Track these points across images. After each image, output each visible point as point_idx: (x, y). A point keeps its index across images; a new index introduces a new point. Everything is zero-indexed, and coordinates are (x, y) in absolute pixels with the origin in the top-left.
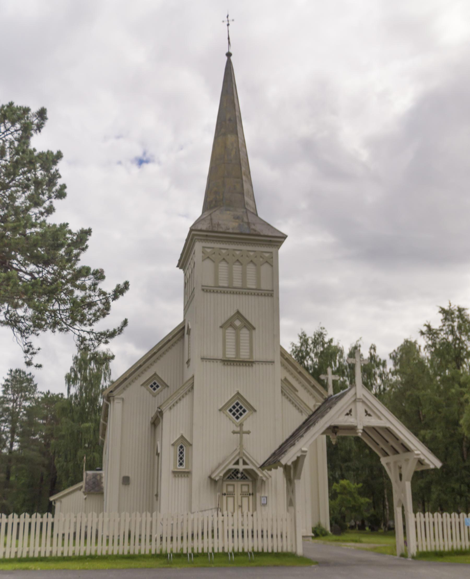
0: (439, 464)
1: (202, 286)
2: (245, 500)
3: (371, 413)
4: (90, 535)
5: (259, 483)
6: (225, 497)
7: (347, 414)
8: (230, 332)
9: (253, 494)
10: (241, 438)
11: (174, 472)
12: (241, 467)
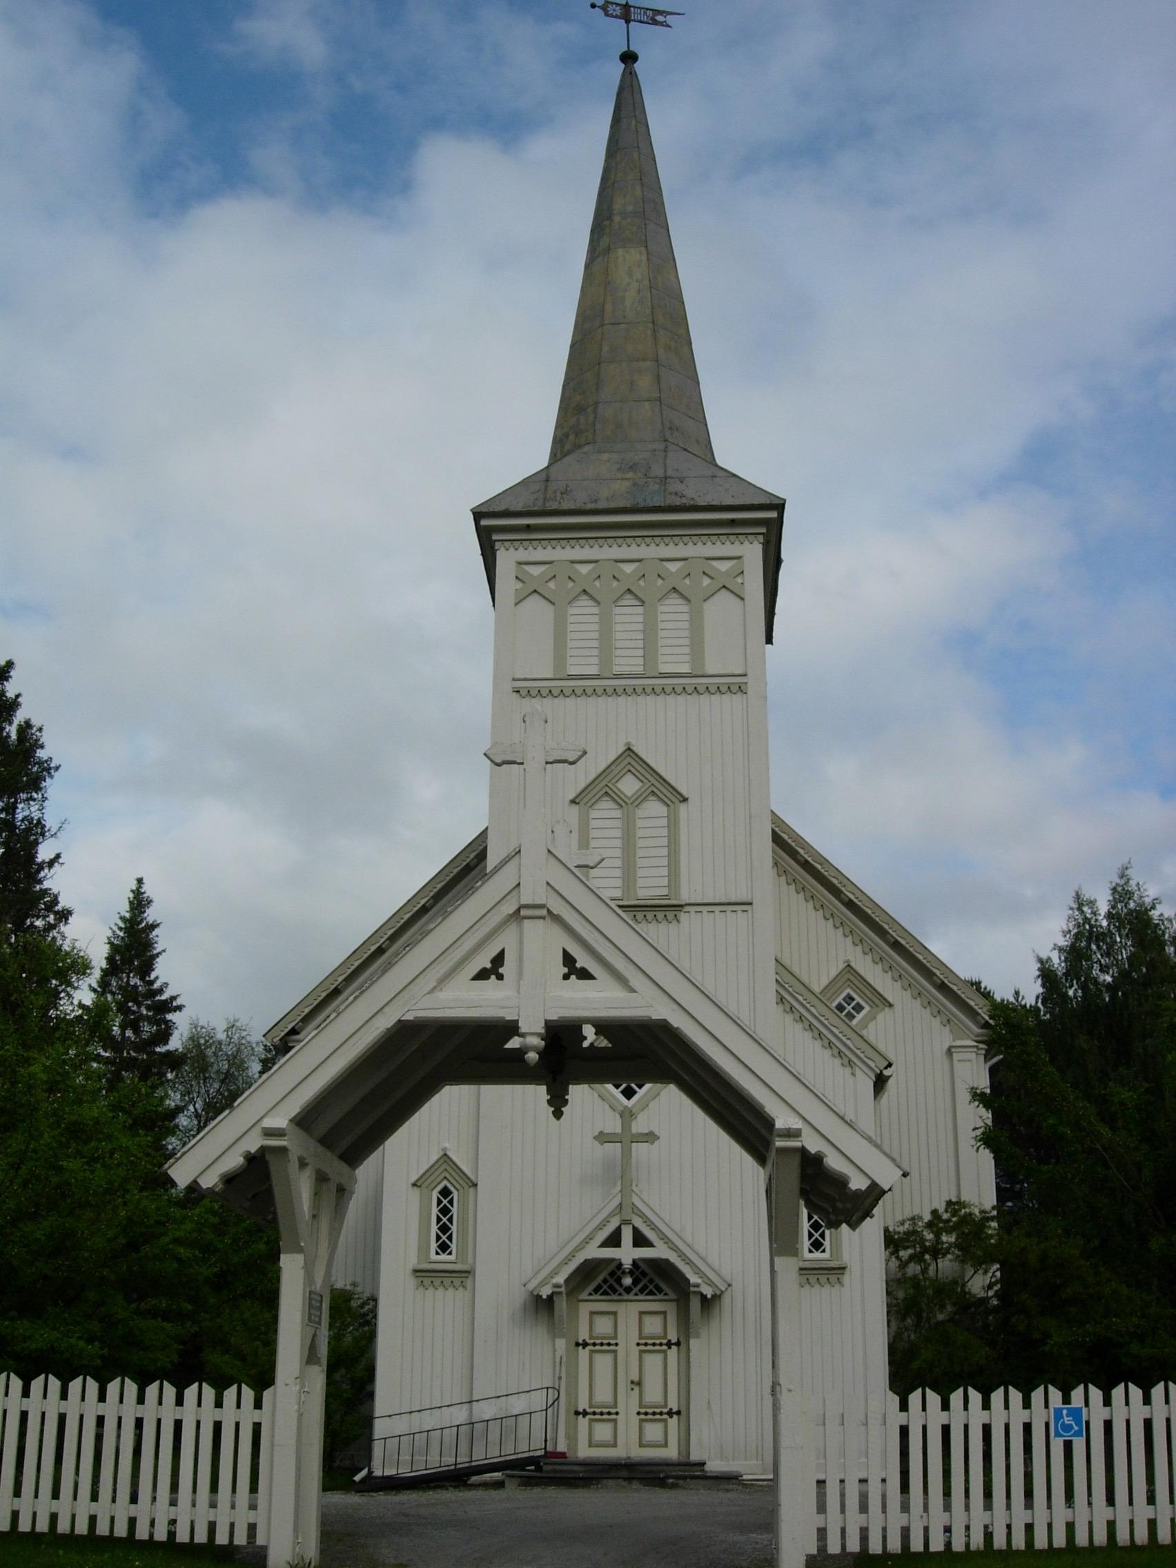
0: (182, 1173)
1: (514, 680)
2: (653, 1362)
3: (593, 967)
4: (151, 1477)
5: (695, 1304)
6: (583, 1354)
7: (482, 975)
8: (605, 814)
9: (678, 1344)
10: (626, 1154)
11: (415, 1271)
12: (627, 1254)
